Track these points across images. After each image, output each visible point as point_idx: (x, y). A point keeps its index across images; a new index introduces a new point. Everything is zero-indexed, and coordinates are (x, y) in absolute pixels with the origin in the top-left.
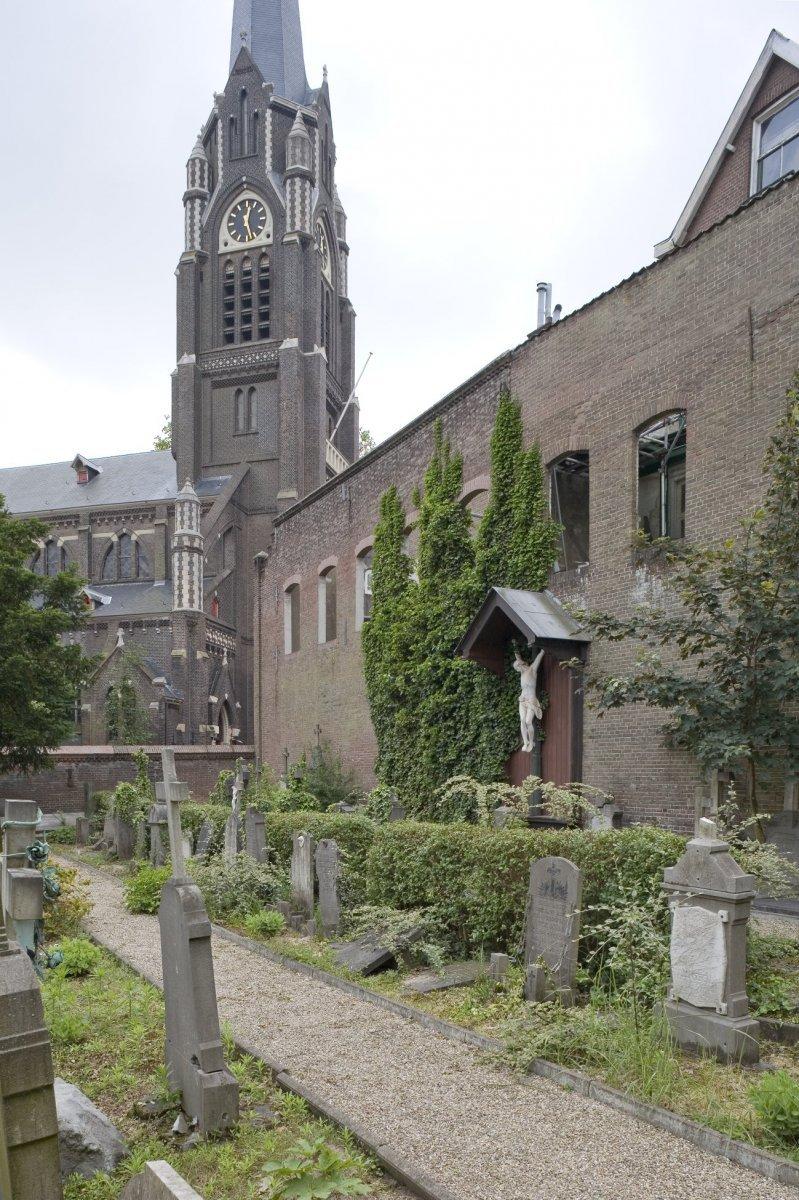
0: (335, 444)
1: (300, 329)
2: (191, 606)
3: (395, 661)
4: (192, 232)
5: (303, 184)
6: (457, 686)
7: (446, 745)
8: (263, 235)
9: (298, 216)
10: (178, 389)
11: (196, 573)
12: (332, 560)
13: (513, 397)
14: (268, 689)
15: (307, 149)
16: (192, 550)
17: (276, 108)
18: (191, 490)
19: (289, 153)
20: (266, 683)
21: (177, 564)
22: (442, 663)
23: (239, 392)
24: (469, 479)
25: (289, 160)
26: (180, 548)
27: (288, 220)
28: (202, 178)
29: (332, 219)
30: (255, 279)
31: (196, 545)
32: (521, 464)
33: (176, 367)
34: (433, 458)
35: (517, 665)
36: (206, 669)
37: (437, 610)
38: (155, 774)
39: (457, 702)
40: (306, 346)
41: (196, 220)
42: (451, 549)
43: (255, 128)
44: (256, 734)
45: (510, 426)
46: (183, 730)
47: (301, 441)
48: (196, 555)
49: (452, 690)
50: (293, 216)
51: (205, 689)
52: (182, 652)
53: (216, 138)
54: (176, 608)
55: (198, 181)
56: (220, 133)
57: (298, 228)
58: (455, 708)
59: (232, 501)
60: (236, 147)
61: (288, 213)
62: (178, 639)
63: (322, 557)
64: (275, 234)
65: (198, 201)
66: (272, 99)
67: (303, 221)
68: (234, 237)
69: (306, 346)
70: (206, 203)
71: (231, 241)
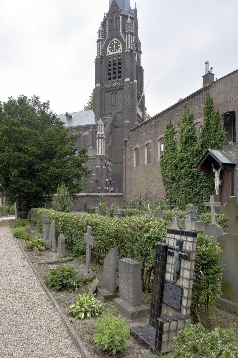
0: (138, 106)
2: (102, 154)
4: (99, 50)
5: (131, 35)
6: (194, 176)
7: (189, 192)
8: (119, 50)
10: (95, 93)
11: (103, 145)
13: (211, 97)
15: (131, 26)
16: (102, 138)
17: (123, 15)
18: (101, 122)
20: (127, 176)
21: (98, 142)
22: (189, 170)
23: (112, 93)
24: (196, 119)
25: (127, 29)
26: (99, 138)
27: (126, 46)
28: (102, 36)
29: (137, 44)
30: (117, 62)
31: (103, 137)
32: (214, 115)
33: (94, 87)
34: (183, 113)
35: (214, 170)
37: (186, 155)
38: (97, 201)
39: (193, 181)
40: (132, 80)
41: (101, 47)
42: (191, 138)
43: (117, 21)
45: (210, 105)
46: (99, 189)
47: (130, 106)
48: (103, 140)
49: (192, 177)
50: (128, 45)
51: (105, 177)
52: (99, 167)
54: (97, 154)
55: (101, 36)
56: (107, 23)
58: (192, 183)
59: (111, 124)
61: (126, 44)
63: (146, 140)
64: (122, 50)
66: (122, 13)
67: (131, 46)
68: (111, 51)
69: (132, 80)
70: (103, 42)
71: (110, 52)
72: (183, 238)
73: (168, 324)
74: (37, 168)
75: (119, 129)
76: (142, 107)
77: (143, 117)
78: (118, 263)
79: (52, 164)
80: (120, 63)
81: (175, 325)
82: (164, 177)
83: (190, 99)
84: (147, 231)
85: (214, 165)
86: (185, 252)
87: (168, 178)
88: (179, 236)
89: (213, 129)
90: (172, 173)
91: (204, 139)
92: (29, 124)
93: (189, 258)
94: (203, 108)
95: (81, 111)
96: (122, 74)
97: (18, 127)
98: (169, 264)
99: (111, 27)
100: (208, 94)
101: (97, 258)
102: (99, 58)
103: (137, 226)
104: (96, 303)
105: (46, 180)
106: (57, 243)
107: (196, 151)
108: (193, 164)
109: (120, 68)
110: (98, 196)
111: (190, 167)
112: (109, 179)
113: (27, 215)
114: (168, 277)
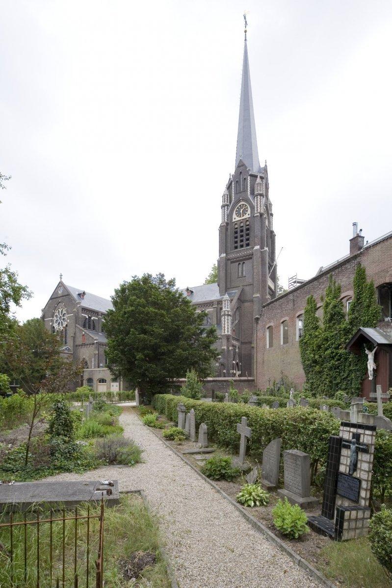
0: (270, 277)
1: (260, 243)
4: (224, 216)
6: (341, 358)
7: (335, 377)
8: (247, 215)
9: (259, 207)
12: (287, 318)
13: (362, 266)
14: (260, 360)
16: (228, 315)
17: (252, 176)
19: (256, 188)
20: (258, 357)
24: (344, 292)
25: (256, 190)
26: (225, 315)
28: (227, 200)
29: (268, 207)
30: (244, 228)
35: (367, 352)
36: (232, 353)
37: (332, 334)
40: (262, 248)
41: (226, 213)
44: (255, 373)
45: (361, 275)
47: (261, 278)
49: (339, 360)
50: (257, 207)
51: (232, 359)
52: (225, 347)
53: (232, 187)
54: (223, 334)
56: (233, 185)
57: (259, 211)
60: (238, 189)
61: (256, 207)
62: (223, 343)
63: (282, 317)
64: (251, 214)
65: (226, 207)
68: (238, 216)
69: (262, 248)
72: (360, 431)
73: (349, 512)
74: (163, 350)
75: (246, 304)
76: (274, 278)
77: (275, 289)
78: (281, 456)
79: (178, 347)
80: (248, 230)
81: (355, 515)
82: (304, 359)
83: (336, 269)
84: (311, 423)
85: (367, 346)
86: (363, 444)
87: (309, 360)
88: (356, 429)
89: (365, 304)
90: (314, 355)
91: (353, 316)
92: (155, 304)
93: (368, 450)
94: (353, 279)
95: (202, 285)
96: (250, 242)
97: (144, 308)
98: (343, 456)
100: (359, 263)
101: (254, 450)
102: (224, 225)
103: (301, 417)
104: (260, 491)
105: (171, 364)
106: (197, 432)
107: (344, 330)
108: (340, 345)
109: (248, 235)
110: (227, 381)
111: (337, 348)
112: (236, 361)
113: (151, 401)
114: (343, 469)
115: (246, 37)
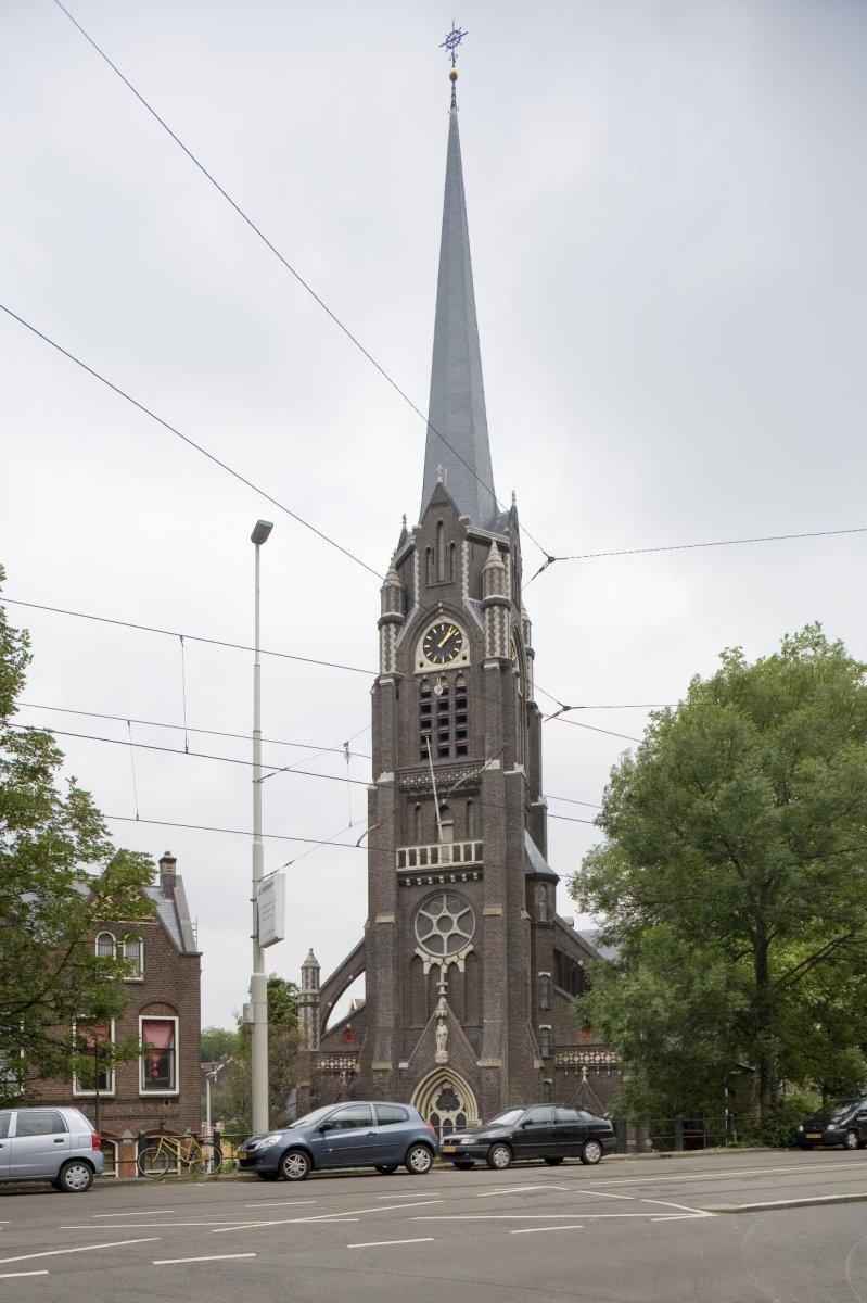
3: (628, 906)
5: (502, 611)
8: (459, 657)
17: (472, 538)
29: (520, 635)
40: (507, 765)
56: (416, 562)
57: (497, 654)
61: (488, 639)
66: (468, 531)
68: (430, 658)
69: (507, 765)
71: (427, 662)
80: (461, 703)
99: (430, 573)
115: (454, 95)
